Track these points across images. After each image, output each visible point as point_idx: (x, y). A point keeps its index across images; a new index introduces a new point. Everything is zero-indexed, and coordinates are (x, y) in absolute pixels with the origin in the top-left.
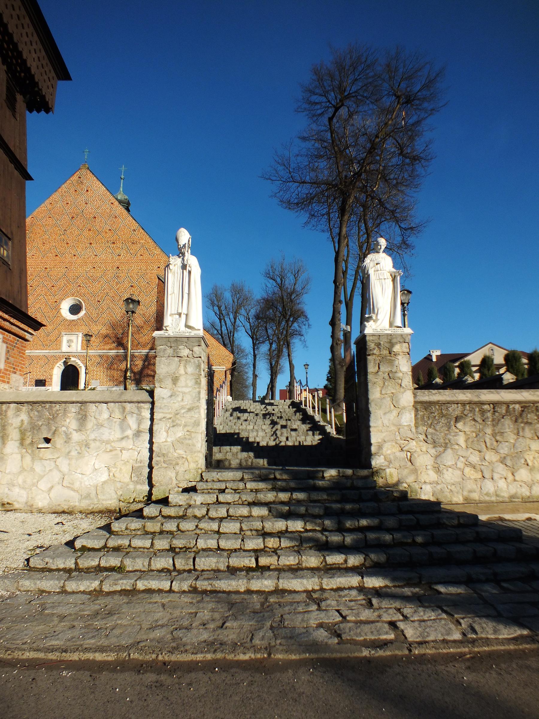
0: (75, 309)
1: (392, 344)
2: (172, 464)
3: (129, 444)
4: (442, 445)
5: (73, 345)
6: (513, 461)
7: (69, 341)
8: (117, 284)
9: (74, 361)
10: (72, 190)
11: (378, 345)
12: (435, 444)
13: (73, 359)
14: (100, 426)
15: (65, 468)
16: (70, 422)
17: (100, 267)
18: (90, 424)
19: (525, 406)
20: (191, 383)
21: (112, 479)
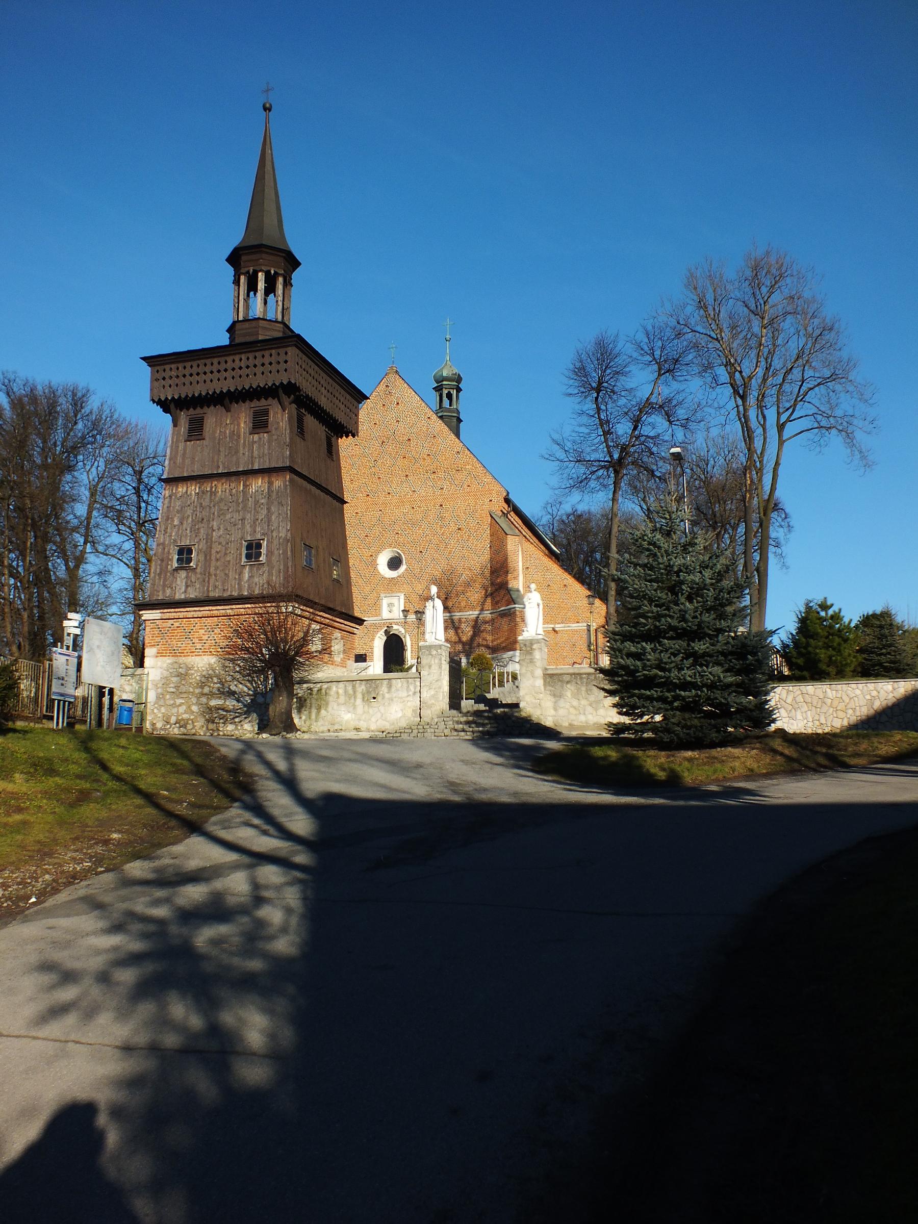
0: (394, 563)
1: (532, 644)
2: (430, 707)
3: (410, 698)
4: (557, 696)
5: (395, 609)
7: (390, 605)
8: (441, 527)
9: (397, 629)
10: (380, 405)
11: (525, 645)
12: (554, 695)
13: (395, 627)
14: (397, 690)
15: (383, 711)
16: (384, 689)
17: (419, 507)
18: (393, 689)
20: (437, 668)
21: (404, 716)
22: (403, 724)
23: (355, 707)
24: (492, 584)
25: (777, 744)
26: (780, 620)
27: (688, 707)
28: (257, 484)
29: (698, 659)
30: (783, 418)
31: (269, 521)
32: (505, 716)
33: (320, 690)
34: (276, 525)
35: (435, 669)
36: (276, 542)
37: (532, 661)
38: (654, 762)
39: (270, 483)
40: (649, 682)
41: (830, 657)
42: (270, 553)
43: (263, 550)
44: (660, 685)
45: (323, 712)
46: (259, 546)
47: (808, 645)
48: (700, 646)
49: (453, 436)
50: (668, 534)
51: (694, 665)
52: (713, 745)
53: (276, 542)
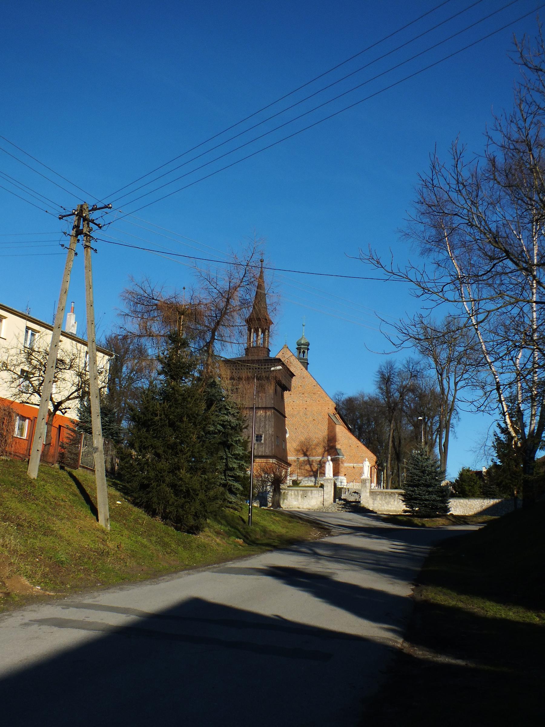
2: (327, 501)
4: (374, 499)
6: (388, 503)
16: (309, 494)
19: (392, 493)
22: (316, 507)
23: (298, 499)
24: (328, 446)
25: (451, 518)
26: (452, 473)
27: (426, 506)
28: (261, 413)
29: (430, 493)
30: (457, 379)
31: (265, 427)
32: (355, 505)
33: (284, 493)
34: (268, 429)
35: (329, 487)
36: (268, 436)
37: (366, 486)
38: (417, 521)
39: (266, 413)
40: (416, 499)
41: (470, 489)
42: (265, 440)
43: (263, 438)
44: (419, 500)
45: (285, 501)
46: (261, 436)
47: (462, 484)
48: (430, 489)
49: (304, 369)
50: (421, 455)
51: (429, 494)
52: (433, 517)
53: (268, 436)
